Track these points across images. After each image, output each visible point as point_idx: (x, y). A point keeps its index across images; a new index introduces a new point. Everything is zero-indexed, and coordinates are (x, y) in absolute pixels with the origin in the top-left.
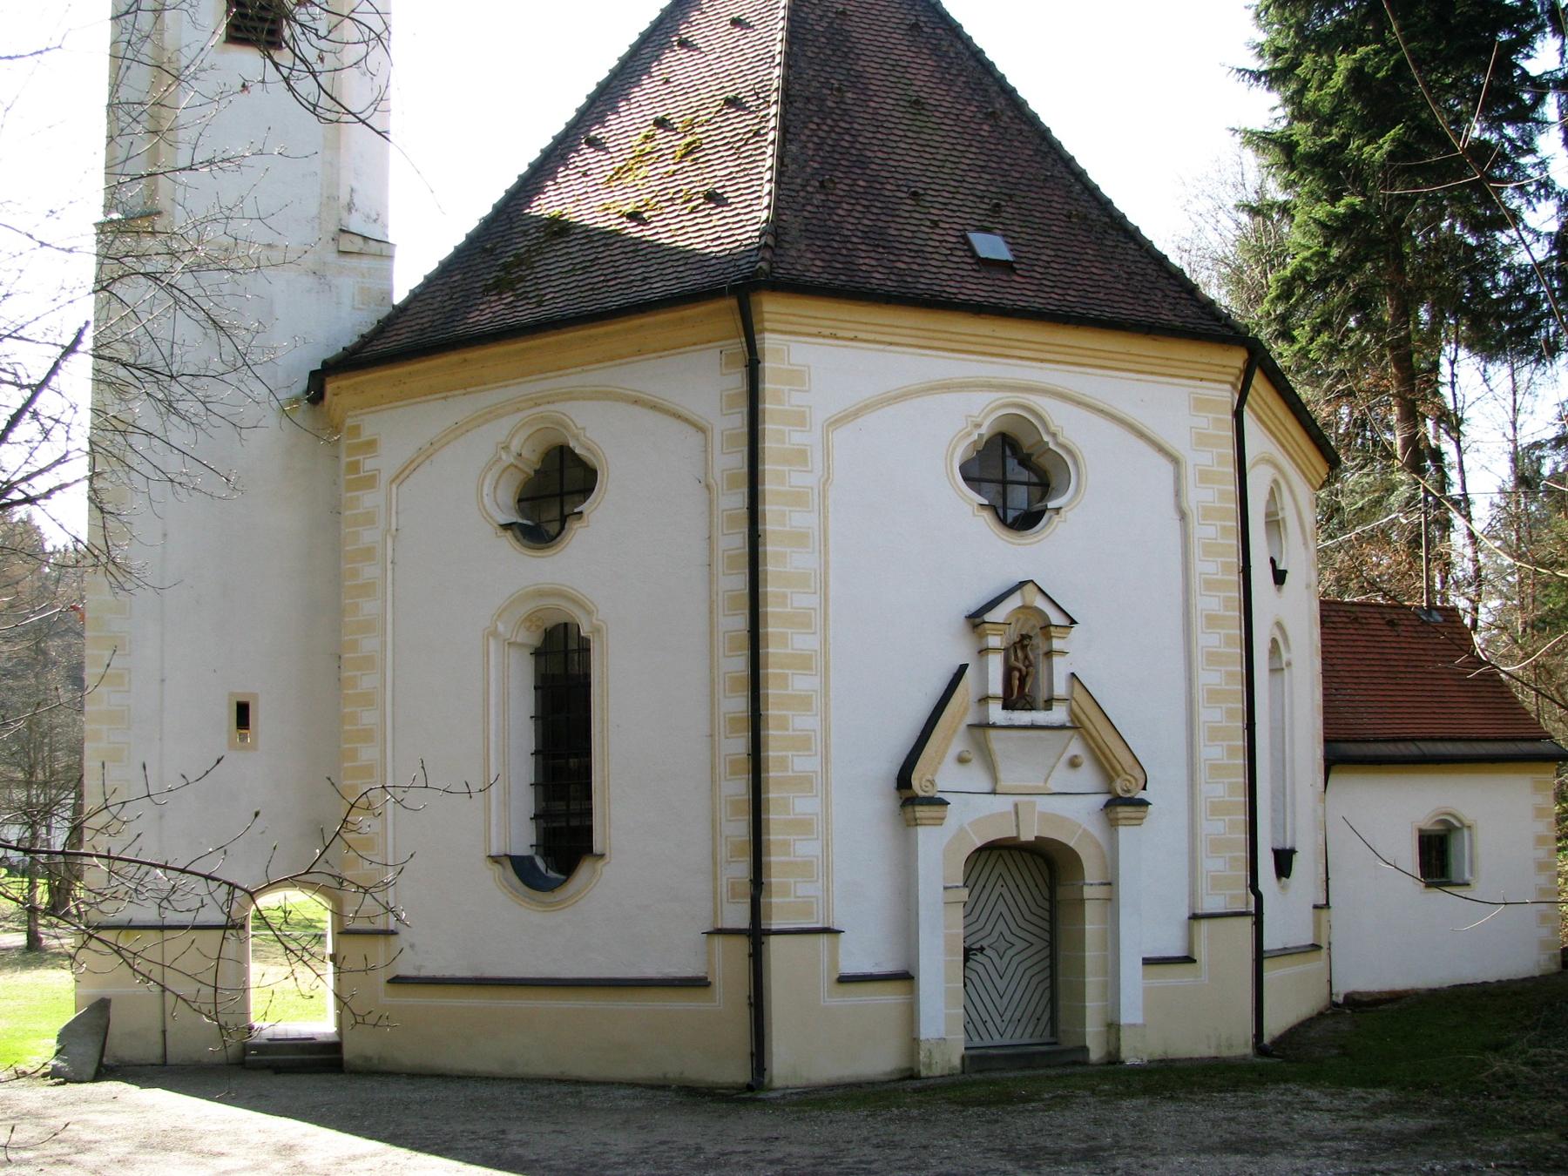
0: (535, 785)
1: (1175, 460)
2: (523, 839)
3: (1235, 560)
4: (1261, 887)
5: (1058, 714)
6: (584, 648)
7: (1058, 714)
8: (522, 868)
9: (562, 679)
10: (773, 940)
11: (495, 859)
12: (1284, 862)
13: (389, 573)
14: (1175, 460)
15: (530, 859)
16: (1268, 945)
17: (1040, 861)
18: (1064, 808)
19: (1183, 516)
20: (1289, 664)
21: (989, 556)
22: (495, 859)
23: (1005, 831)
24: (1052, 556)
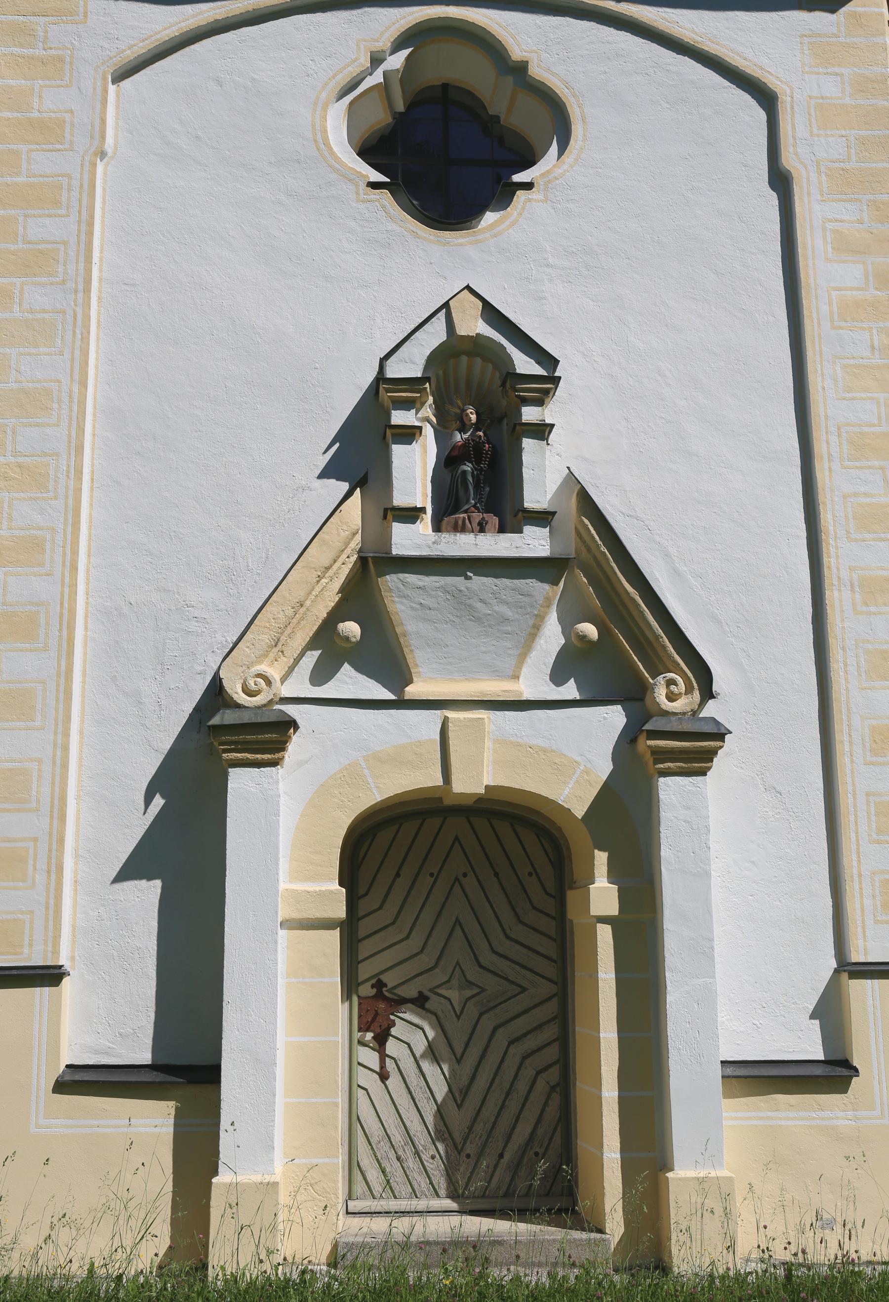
1: (766, 98)
7: (534, 542)
14: (766, 98)
18: (566, 755)
19: (780, 181)
21: (393, 285)
24: (517, 261)
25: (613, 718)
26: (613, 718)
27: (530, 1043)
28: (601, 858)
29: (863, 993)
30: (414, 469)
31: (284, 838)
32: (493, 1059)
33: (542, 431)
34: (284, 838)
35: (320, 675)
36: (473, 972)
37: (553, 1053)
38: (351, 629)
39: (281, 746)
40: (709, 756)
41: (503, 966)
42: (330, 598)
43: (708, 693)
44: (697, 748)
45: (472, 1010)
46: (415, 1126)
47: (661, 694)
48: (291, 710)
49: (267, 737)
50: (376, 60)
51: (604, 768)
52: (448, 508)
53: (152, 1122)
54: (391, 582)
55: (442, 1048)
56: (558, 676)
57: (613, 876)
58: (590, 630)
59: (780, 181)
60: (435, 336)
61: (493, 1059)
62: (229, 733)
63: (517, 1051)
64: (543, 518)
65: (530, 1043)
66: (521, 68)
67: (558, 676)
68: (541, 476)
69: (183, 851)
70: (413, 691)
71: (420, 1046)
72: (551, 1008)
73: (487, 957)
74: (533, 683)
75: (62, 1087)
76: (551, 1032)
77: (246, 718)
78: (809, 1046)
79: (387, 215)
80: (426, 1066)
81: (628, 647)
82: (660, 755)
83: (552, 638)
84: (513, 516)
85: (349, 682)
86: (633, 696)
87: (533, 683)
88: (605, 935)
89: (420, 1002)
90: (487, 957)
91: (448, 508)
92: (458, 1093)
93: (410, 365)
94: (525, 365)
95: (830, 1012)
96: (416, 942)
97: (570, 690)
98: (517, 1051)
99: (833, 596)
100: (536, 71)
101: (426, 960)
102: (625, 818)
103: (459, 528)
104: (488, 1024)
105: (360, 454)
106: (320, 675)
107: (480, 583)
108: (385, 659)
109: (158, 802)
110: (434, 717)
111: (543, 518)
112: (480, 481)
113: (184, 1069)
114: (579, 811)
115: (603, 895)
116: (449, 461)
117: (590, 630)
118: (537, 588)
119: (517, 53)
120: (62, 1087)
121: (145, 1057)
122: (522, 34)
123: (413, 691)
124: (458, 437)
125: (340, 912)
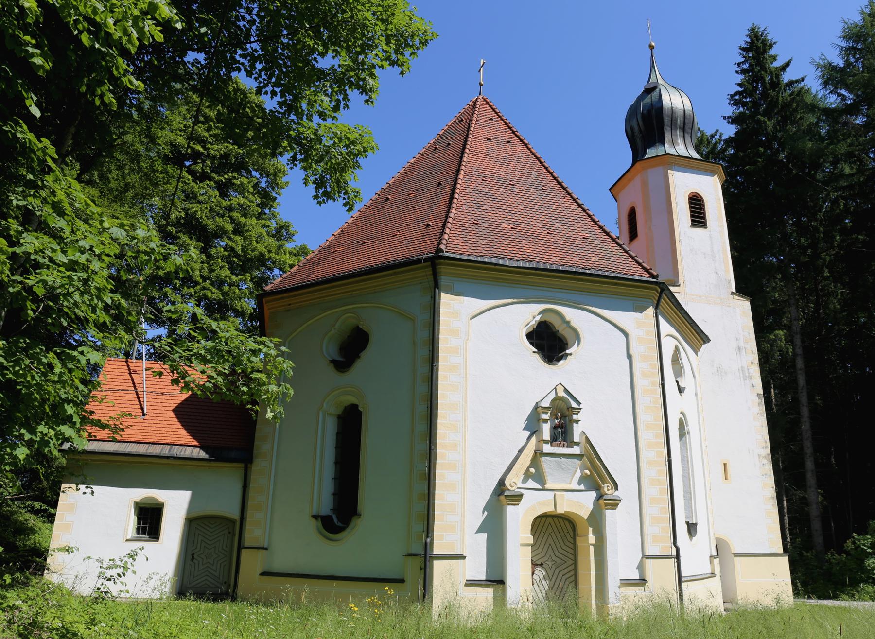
0: (334, 494)
1: (626, 335)
2: (326, 507)
3: (658, 380)
4: (678, 544)
5: (576, 450)
6: (360, 414)
7: (576, 450)
8: (334, 362)
9: (350, 423)
10: (436, 563)
11: (315, 517)
12: (692, 528)
13: (272, 483)
14: (626, 335)
15: (330, 517)
16: (684, 573)
17: (567, 523)
18: (581, 504)
19: (629, 357)
20: (688, 433)
21: (541, 380)
22: (315, 517)
23: (549, 509)
24: (568, 374)
25: (593, 495)
26: (593, 495)
27: (567, 576)
28: (591, 529)
29: (648, 562)
30: (546, 430)
31: (519, 522)
32: (559, 580)
33: (577, 422)
34: (519, 522)
35: (524, 481)
36: (554, 558)
37: (573, 578)
38: (532, 470)
39: (519, 501)
40: (617, 505)
41: (561, 556)
42: (529, 463)
43: (617, 489)
44: (614, 504)
45: (554, 567)
46: (540, 596)
47: (606, 489)
48: (523, 491)
49: (517, 498)
50: (534, 318)
51: (591, 507)
52: (554, 440)
53: (488, 594)
54: (543, 459)
55: (547, 577)
56: (579, 484)
57: (593, 534)
58: (588, 472)
59: (629, 357)
60: (552, 396)
61: (559, 580)
62: (502, 496)
63: (564, 578)
64: (578, 444)
65: (567, 576)
66: (568, 322)
67: (579, 484)
68: (577, 431)
69: (494, 526)
70: (547, 486)
71: (542, 577)
72: (573, 567)
73: (557, 554)
74: (575, 485)
75: (466, 585)
76: (572, 573)
77: (513, 493)
78: (636, 576)
79: (537, 360)
80: (543, 582)
81: (597, 477)
82: (606, 505)
83: (578, 474)
84: (571, 444)
85: (531, 484)
86: (597, 488)
87: (575, 485)
88: (592, 548)
89: (541, 565)
90: (557, 554)
91: (554, 440)
92: (551, 588)
93: (546, 403)
94: (574, 405)
95: (641, 567)
96: (540, 549)
97: (582, 487)
98: (564, 578)
99: (642, 465)
100: (572, 324)
101: (543, 554)
102: (596, 520)
103: (558, 446)
104: (557, 571)
105: (533, 425)
106: (524, 481)
107: (563, 460)
108: (540, 478)
109: (486, 513)
110: (553, 493)
111: (578, 444)
112: (562, 432)
113: (496, 581)
114: (586, 518)
115: (592, 539)
116: (554, 428)
117: (588, 472)
118: (577, 462)
119: (568, 319)
120: (466, 585)
121: (484, 578)
122: (571, 314)
123: (547, 486)
124: (556, 421)
125: (532, 542)
